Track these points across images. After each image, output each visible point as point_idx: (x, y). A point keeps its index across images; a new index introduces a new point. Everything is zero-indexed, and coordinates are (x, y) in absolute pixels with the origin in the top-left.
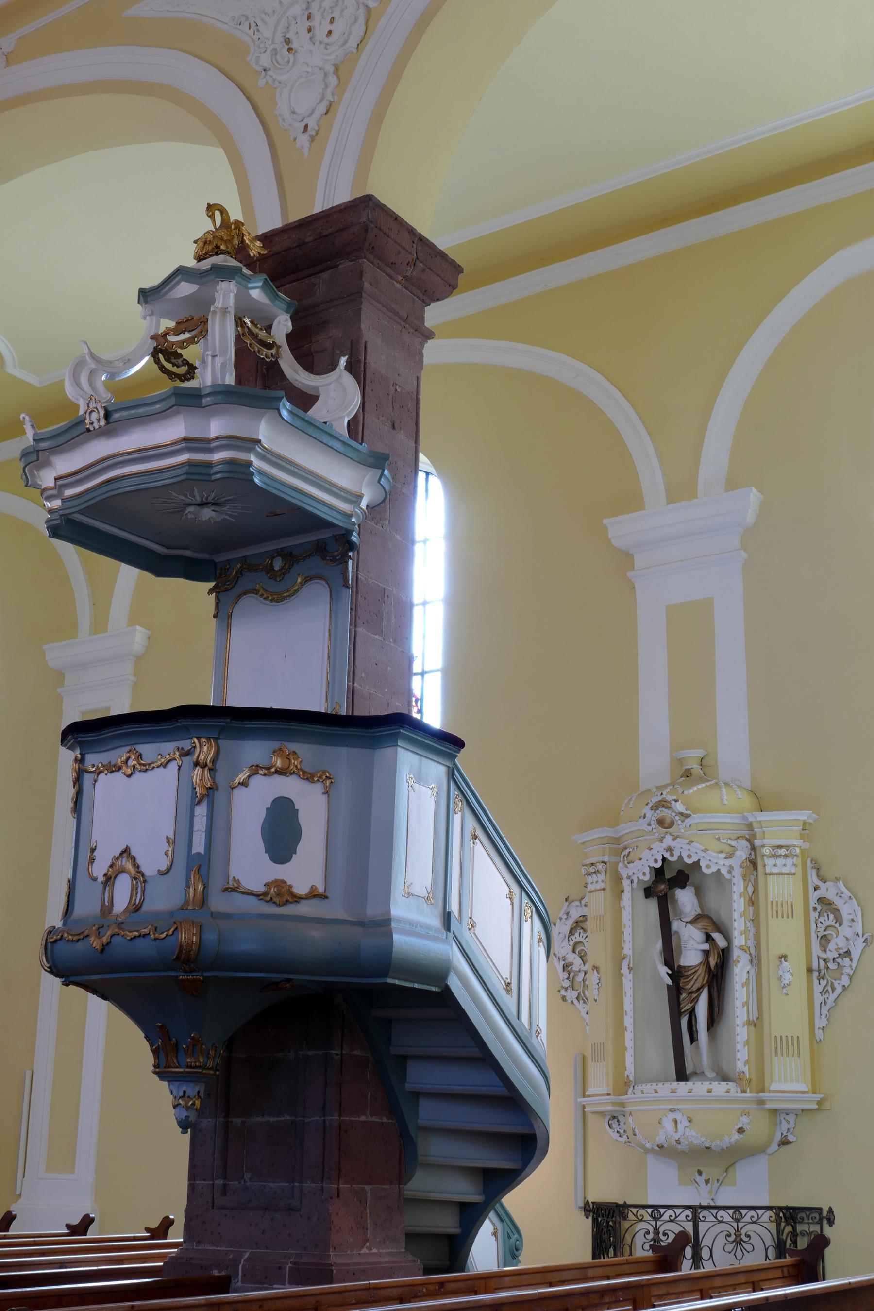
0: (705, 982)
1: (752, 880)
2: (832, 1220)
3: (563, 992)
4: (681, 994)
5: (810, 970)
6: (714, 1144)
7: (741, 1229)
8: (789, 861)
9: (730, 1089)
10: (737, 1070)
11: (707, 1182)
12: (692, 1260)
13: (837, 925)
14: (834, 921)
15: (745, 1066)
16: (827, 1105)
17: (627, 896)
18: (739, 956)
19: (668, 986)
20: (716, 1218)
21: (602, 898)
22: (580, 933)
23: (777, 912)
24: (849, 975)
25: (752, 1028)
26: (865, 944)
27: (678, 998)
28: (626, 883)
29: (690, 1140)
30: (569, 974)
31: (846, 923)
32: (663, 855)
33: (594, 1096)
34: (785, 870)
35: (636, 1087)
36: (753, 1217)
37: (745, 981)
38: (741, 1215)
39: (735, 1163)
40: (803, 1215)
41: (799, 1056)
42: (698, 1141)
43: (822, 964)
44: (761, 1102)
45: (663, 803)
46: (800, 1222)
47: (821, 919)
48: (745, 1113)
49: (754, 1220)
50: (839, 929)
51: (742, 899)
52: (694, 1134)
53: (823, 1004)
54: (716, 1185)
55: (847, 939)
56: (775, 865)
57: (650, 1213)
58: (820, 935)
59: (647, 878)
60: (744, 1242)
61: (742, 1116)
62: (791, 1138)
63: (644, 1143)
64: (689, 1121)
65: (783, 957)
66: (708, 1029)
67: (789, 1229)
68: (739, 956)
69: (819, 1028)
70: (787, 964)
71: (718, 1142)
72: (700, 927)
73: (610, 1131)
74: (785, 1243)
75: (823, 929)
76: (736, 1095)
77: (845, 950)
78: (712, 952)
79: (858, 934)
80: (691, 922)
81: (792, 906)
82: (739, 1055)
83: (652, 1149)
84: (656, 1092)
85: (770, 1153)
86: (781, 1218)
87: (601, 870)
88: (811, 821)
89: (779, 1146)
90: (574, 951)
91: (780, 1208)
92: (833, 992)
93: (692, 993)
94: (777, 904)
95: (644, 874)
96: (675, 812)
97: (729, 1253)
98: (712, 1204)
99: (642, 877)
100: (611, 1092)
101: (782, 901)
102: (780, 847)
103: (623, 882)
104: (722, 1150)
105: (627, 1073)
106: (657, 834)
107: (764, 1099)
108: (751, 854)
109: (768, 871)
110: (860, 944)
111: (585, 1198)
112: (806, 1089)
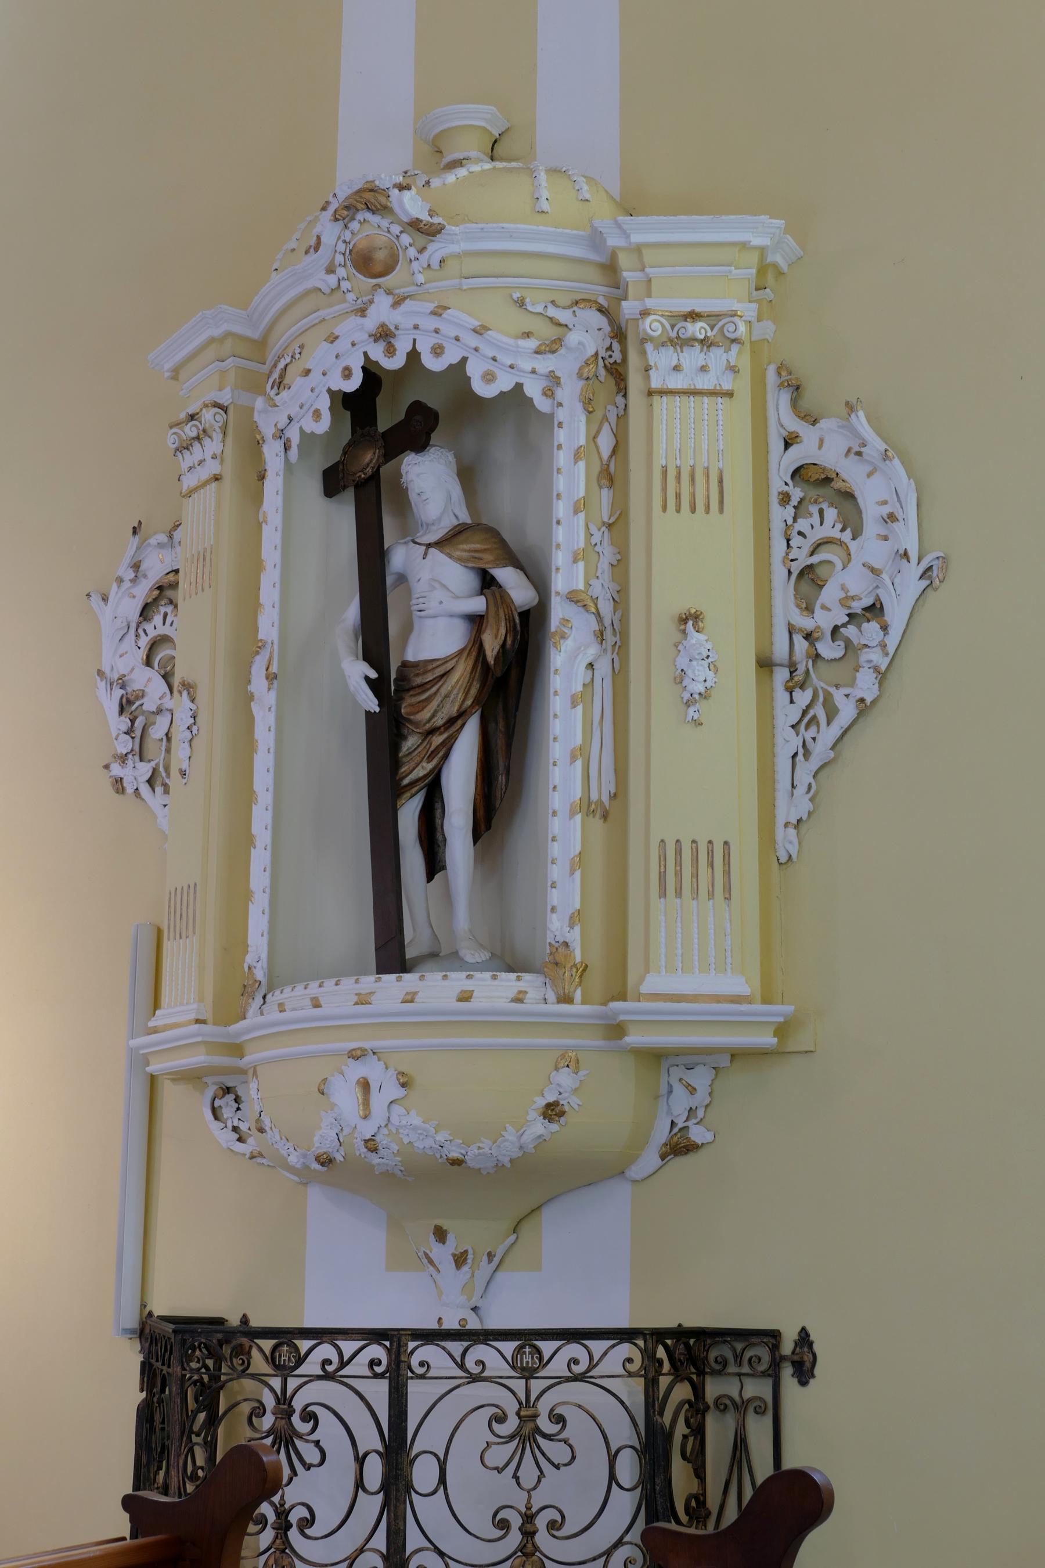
0: (469, 702)
1: (613, 419)
2: (808, 1365)
3: (116, 770)
4: (404, 738)
5: (765, 664)
6: (473, 1151)
7: (538, 1398)
8: (717, 358)
9: (526, 992)
10: (550, 939)
11: (460, 1260)
12: (380, 1497)
13: (846, 537)
14: (839, 526)
15: (572, 926)
16: (801, 1041)
17: (274, 484)
18: (565, 621)
19: (368, 714)
20: (462, 1366)
21: (213, 504)
22: (165, 615)
23: (678, 496)
24: (876, 669)
25: (597, 823)
26: (925, 583)
27: (395, 747)
28: (272, 454)
29: (406, 1141)
30: (133, 721)
31: (871, 527)
32: (365, 354)
33: (167, 1028)
34: (704, 383)
35: (269, 996)
36: (576, 1362)
37: (580, 688)
38: (541, 1359)
39: (539, 1208)
40: (726, 1351)
41: (728, 899)
42: (428, 1143)
43: (801, 645)
44: (616, 1030)
45: (368, 196)
46: (714, 1373)
47: (802, 525)
48: (568, 1061)
49: (578, 1369)
50: (853, 546)
51: (582, 464)
52: (417, 1121)
53: (800, 757)
54: (485, 1269)
55: (874, 571)
56: (677, 368)
57: (268, 1352)
58: (796, 567)
59: (323, 426)
60: (545, 1436)
61: (557, 1069)
62: (697, 1134)
63: (284, 1153)
64: (403, 1085)
65: (690, 619)
66: (477, 836)
67: (682, 1392)
68: (565, 621)
69: (786, 825)
70: (701, 637)
71: (486, 1144)
72: (465, 555)
73: (215, 1125)
74: (669, 1436)
75: (807, 545)
76: (543, 1007)
77: (868, 602)
78: (491, 620)
79: (906, 554)
80: (439, 544)
81: (721, 481)
82: (554, 897)
83: (306, 1167)
84: (317, 1005)
85: (638, 1177)
86: (660, 1362)
87: (212, 426)
88: (778, 259)
89: (663, 1157)
90: (148, 662)
91: (658, 1335)
92: (828, 724)
93: (432, 732)
94: (679, 474)
95: (317, 415)
96: (400, 222)
97: (499, 1470)
98: (473, 1324)
99: (310, 426)
100: (208, 1015)
101: (693, 467)
102: (693, 316)
103: (265, 449)
104: (499, 1166)
105: (249, 959)
106: (351, 297)
107: (622, 1018)
108: (610, 348)
109: (655, 384)
110: (911, 584)
111: (143, 1306)
112: (745, 990)
